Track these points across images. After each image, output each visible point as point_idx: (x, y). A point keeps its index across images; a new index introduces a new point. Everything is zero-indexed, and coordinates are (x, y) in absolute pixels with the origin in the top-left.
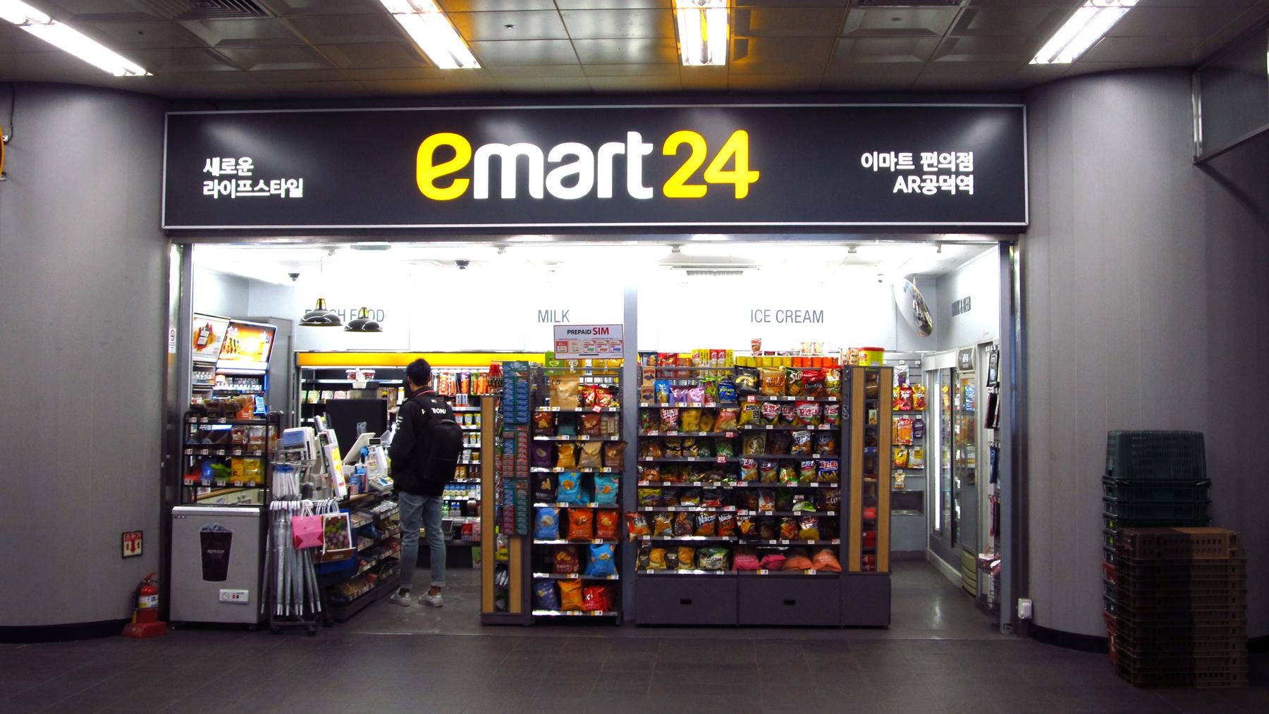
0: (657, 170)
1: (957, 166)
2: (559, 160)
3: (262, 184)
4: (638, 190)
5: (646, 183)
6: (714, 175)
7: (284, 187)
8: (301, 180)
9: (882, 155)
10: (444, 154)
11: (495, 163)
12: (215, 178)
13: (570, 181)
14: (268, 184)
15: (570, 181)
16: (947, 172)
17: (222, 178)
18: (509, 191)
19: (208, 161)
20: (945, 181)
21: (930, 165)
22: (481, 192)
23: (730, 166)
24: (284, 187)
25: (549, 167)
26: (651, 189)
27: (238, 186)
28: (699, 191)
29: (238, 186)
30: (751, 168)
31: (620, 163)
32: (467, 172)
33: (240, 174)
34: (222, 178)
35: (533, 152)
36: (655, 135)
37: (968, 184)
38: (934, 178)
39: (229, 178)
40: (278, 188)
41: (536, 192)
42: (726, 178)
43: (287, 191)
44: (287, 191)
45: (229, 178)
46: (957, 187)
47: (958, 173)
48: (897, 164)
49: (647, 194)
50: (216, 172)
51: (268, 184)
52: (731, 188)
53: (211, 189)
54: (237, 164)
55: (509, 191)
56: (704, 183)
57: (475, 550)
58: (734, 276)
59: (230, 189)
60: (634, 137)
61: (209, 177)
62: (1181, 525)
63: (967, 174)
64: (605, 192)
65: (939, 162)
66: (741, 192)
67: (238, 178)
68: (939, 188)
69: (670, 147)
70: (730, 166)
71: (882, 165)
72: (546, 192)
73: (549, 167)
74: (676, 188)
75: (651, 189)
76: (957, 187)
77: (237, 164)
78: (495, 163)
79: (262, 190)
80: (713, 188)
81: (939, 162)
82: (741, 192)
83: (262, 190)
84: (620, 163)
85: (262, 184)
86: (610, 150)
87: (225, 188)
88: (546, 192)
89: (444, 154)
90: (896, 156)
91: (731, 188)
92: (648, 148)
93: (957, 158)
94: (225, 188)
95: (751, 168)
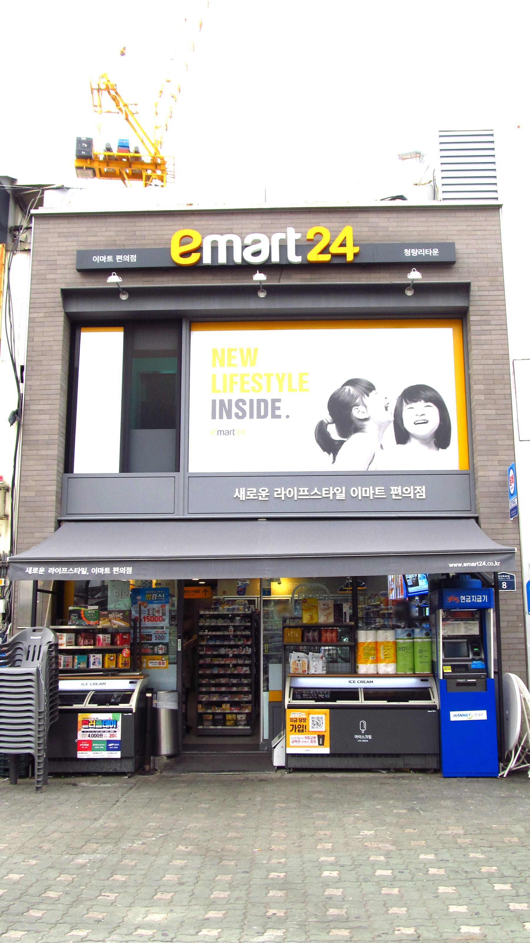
3: (316, 491)
5: (297, 254)
6: (335, 249)
7: (79, 570)
8: (344, 488)
9: (364, 489)
13: (257, 254)
14: (320, 490)
15: (257, 254)
19: (237, 490)
21: (119, 260)
23: (343, 245)
24: (79, 570)
25: (244, 247)
26: (300, 257)
27: (299, 491)
28: (326, 258)
29: (299, 491)
32: (199, 249)
42: (342, 250)
51: (320, 490)
52: (344, 256)
56: (329, 253)
62: (91, 649)
65: (123, 259)
71: (101, 260)
73: (244, 247)
74: (314, 256)
75: (300, 257)
79: (71, 571)
80: (334, 256)
81: (123, 259)
82: (350, 258)
83: (71, 571)
85: (316, 491)
86: (276, 238)
90: (107, 257)
91: (344, 256)
93: (130, 257)
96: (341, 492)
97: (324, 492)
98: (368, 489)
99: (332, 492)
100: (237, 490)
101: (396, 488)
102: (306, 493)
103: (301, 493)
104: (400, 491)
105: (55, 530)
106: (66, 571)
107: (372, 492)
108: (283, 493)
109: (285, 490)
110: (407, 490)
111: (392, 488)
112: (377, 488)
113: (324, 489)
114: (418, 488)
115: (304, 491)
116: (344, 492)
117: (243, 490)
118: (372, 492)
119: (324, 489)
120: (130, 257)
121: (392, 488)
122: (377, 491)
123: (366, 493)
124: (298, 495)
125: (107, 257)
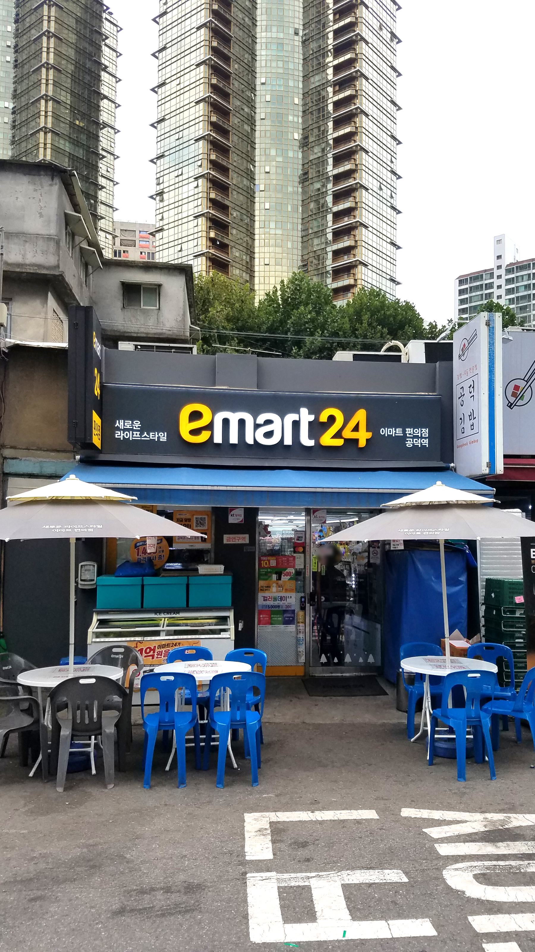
0: (317, 428)
1: (421, 434)
2: (262, 423)
3: (145, 434)
4: (306, 441)
5: (310, 437)
6: (348, 434)
7: (157, 436)
8: (166, 433)
9: (389, 430)
10: (195, 416)
11: (226, 422)
12: (121, 429)
14: (148, 434)
15: (269, 435)
16: (417, 437)
17: (124, 430)
18: (234, 439)
19: (118, 421)
20: (416, 441)
21: (410, 434)
22: (218, 439)
23: (356, 429)
25: (257, 426)
27: (133, 434)
28: (339, 442)
29: (133, 434)
30: (368, 430)
31: (296, 425)
32: (210, 427)
33: (134, 428)
34: (124, 430)
35: (248, 417)
36: (315, 410)
37: (426, 442)
38: (411, 440)
39: (128, 430)
40: (153, 436)
41: (250, 440)
43: (159, 438)
44: (159, 438)
45: (128, 430)
46: (421, 443)
47: (422, 438)
48: (395, 433)
49: (311, 443)
50: (122, 427)
51: (148, 434)
52: (356, 441)
53: (119, 435)
54: (133, 423)
55: (234, 439)
57: (228, 619)
58: (173, 356)
59: (129, 435)
60: (304, 411)
61: (118, 429)
63: (425, 438)
64: (288, 441)
65: (414, 433)
66: (362, 443)
67: (133, 430)
68: (413, 444)
69: (324, 417)
70: (356, 429)
72: (255, 440)
73: (257, 426)
76: (421, 443)
77: (133, 423)
78: (226, 422)
79: (145, 437)
80: (347, 441)
81: (414, 433)
82: (362, 443)
83: (145, 437)
84: (296, 425)
85: (145, 434)
86: (290, 418)
87: (127, 435)
88: (255, 440)
89: (195, 416)
90: (395, 430)
91: (356, 441)
92: (312, 418)
93: (421, 431)
94: (127, 435)
95: (368, 430)
96: (164, 436)
97: (151, 436)
98: (391, 430)
99: (157, 436)
100: (118, 421)
101: (409, 429)
102: (138, 436)
103: (135, 436)
104: (412, 432)
105: (352, 431)
106: (138, 436)
107: (394, 432)
108: (122, 435)
109: (123, 433)
110: (416, 431)
111: (407, 429)
112: (397, 429)
113: (151, 434)
114: (424, 430)
115: (136, 434)
116: (166, 436)
117: (122, 422)
118: (394, 432)
119: (151, 434)
120: (421, 431)
121: (407, 429)
122: (397, 431)
123: (390, 432)
124: (132, 437)
125: (395, 430)
